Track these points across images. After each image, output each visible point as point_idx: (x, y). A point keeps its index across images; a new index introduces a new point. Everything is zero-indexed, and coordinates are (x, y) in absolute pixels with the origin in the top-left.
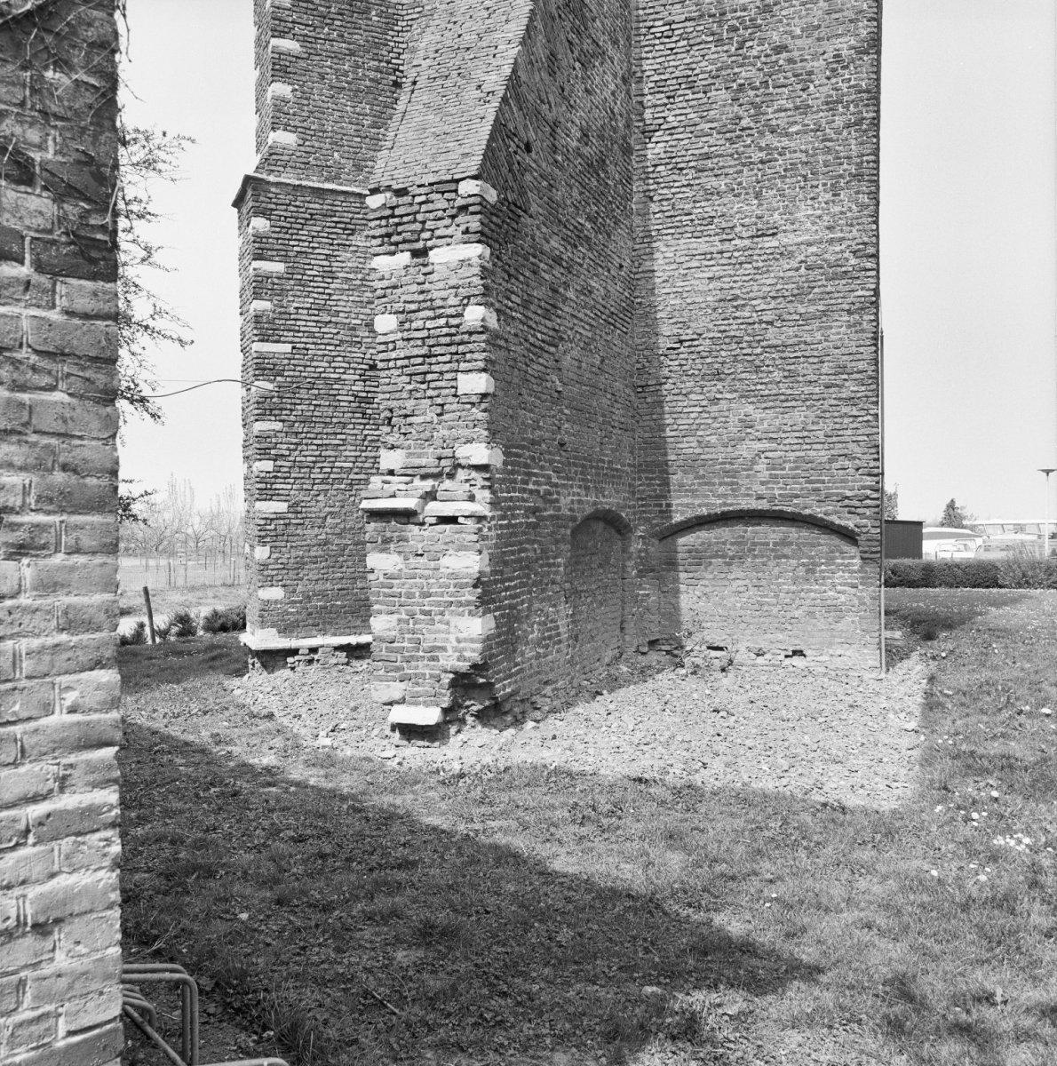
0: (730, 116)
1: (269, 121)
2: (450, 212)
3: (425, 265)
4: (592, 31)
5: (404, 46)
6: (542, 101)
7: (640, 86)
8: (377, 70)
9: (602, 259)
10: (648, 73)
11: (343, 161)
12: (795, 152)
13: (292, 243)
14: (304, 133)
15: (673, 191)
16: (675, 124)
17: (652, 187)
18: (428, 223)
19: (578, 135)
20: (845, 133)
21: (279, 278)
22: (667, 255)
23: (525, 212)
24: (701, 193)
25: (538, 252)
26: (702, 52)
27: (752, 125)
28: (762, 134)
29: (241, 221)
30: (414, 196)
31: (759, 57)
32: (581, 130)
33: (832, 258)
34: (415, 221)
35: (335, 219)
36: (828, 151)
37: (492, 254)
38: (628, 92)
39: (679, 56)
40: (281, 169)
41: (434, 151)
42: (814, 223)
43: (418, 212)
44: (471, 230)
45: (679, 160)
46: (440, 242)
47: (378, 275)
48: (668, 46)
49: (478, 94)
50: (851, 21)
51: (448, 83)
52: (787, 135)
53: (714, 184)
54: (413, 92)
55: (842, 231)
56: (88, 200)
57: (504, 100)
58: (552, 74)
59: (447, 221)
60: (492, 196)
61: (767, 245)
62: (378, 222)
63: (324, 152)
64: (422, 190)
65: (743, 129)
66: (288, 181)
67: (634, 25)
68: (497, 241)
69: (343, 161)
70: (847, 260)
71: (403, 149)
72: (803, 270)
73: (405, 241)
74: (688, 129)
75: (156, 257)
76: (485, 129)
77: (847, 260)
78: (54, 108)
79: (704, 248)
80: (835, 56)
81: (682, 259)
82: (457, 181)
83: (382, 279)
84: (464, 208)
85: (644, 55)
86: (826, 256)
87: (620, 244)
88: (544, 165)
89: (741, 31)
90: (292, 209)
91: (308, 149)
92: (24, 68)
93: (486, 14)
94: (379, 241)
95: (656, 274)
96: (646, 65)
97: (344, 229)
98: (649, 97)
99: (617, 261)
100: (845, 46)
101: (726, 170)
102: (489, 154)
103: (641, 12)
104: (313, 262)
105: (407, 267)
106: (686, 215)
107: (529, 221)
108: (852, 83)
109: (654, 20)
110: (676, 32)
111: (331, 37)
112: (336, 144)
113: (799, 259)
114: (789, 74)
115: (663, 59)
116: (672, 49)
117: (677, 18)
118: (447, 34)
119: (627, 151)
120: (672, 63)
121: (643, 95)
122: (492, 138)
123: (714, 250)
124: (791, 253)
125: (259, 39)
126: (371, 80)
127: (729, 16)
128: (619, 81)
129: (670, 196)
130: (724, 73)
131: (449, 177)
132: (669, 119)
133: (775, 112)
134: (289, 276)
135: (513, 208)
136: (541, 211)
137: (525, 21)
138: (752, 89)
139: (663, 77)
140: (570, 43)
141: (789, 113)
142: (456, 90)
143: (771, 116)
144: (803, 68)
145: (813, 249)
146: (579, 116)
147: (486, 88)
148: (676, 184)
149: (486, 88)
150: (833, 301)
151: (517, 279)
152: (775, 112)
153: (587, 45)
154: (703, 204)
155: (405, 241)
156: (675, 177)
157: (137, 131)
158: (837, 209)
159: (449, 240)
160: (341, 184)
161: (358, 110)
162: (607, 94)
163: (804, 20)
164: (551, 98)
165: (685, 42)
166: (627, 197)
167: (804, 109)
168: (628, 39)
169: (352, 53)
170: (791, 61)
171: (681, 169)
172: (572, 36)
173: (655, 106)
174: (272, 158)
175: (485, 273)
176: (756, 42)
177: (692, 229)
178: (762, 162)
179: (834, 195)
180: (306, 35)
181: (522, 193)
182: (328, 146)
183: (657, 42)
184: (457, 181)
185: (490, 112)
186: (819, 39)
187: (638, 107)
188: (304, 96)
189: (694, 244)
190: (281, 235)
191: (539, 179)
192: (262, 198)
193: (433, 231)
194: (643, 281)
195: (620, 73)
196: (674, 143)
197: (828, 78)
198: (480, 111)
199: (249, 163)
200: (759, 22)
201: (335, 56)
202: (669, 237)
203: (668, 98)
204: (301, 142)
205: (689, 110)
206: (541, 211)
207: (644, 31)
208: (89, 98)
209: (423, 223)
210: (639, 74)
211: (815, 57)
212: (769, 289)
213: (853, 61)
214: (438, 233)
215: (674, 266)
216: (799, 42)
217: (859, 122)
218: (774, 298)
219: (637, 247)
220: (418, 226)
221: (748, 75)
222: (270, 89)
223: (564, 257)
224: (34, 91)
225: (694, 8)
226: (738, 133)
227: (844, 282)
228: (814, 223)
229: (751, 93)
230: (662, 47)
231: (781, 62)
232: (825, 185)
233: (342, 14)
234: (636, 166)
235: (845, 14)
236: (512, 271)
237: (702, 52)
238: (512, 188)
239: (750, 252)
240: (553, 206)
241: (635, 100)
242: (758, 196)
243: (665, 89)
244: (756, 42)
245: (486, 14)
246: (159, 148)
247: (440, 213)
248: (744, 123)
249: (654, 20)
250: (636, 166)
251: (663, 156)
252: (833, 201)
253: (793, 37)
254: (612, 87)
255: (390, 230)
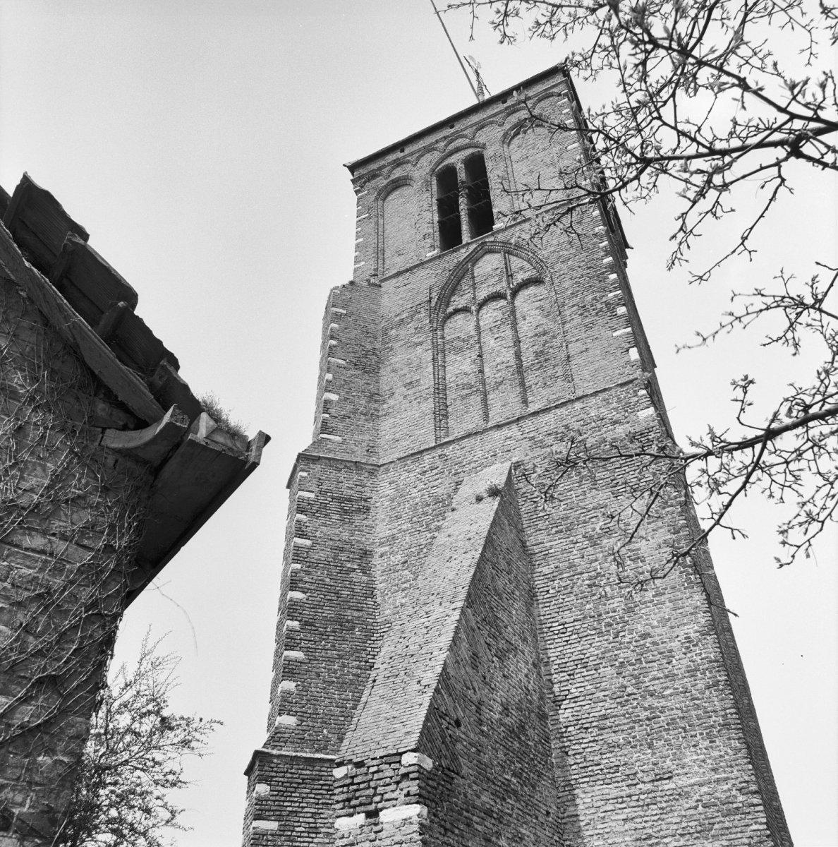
0: (618, 685)
1: (277, 708)
2: (394, 779)
3: (376, 824)
4: (505, 635)
5: (378, 650)
6: (468, 688)
7: (548, 668)
8: (358, 668)
9: (530, 807)
10: (551, 659)
11: (330, 736)
12: (672, 709)
13: (286, 804)
14: (302, 717)
15: (583, 747)
16: (577, 694)
17: (566, 744)
18: (379, 788)
19: (500, 709)
20: (707, 692)
21: (272, 835)
22: (586, 800)
23: (458, 774)
24: (606, 746)
25: (470, 807)
26: (589, 642)
27: (635, 691)
28: (644, 698)
29: (249, 787)
30: (368, 767)
31: (631, 643)
32: (502, 705)
33: (723, 796)
34: (369, 787)
35: (321, 782)
36: (698, 707)
37: (429, 812)
38: (539, 674)
39: (573, 646)
40: (283, 744)
41: (385, 731)
42: (700, 767)
43: (372, 780)
44: (411, 793)
45: (584, 721)
46: (388, 804)
47: (339, 834)
48: (564, 639)
49: (418, 687)
50: (692, 614)
51: (398, 680)
52: (663, 697)
53: (614, 739)
54: (373, 687)
55: (725, 772)
56: (40, 837)
57: (437, 690)
58: (475, 667)
59: (393, 787)
60: (428, 764)
61: (666, 787)
62: (341, 789)
63: (316, 729)
64: (375, 762)
65: (629, 695)
66: (287, 753)
67: (538, 627)
68: (433, 801)
69: (330, 736)
70: (735, 797)
71: (363, 731)
72: (700, 808)
73: (361, 804)
74: (588, 697)
75: (179, 819)
76: (422, 714)
77: (735, 797)
78: (37, 779)
79: (615, 793)
80: (686, 638)
81: (599, 804)
82: (401, 754)
83: (342, 837)
84: (405, 776)
85: (548, 647)
86: (716, 794)
87: (545, 792)
88: (472, 735)
89: (615, 626)
90: (289, 775)
91: (305, 728)
92: (26, 757)
93: (425, 631)
94: (341, 805)
95: (581, 818)
96: (550, 653)
97: (328, 790)
98: (555, 676)
99: (543, 809)
100: (692, 631)
101: (622, 727)
102: (426, 731)
103: (542, 618)
104: (301, 820)
105: (362, 826)
106: (596, 765)
107: (461, 781)
108: (703, 656)
109: (552, 622)
110: (569, 630)
111: (327, 647)
112: (325, 723)
113: (696, 798)
114: (656, 653)
115: (562, 648)
116: (567, 641)
117: (568, 620)
118: (399, 646)
119: (543, 717)
120: (568, 651)
121: (551, 674)
122: (427, 719)
123: (623, 794)
124: (687, 793)
125: (277, 651)
126: (353, 675)
127: (604, 616)
128: (530, 666)
129: (581, 751)
130: (607, 655)
131: (395, 751)
132: (572, 691)
133: (651, 680)
134: (282, 830)
135: (448, 772)
136: (471, 772)
137: (452, 634)
138: (630, 665)
139: (563, 661)
140: (489, 645)
141: (662, 681)
142: (403, 685)
143: (648, 684)
144: (665, 648)
145: (704, 789)
146: (500, 696)
147: (424, 682)
148: (585, 741)
149: (424, 682)
150: (733, 836)
151: (453, 832)
152: (651, 680)
153: (502, 644)
154: (608, 755)
155: (361, 804)
156: (584, 735)
157: (182, 718)
158: (716, 754)
159: (394, 802)
160: (327, 754)
161: (343, 697)
162: (521, 676)
163: (658, 615)
164: (475, 684)
165: (576, 636)
166: (547, 754)
167: (672, 677)
168: (535, 636)
169: (340, 657)
170: (654, 643)
171: (587, 728)
172: (489, 640)
173: (561, 682)
174: (277, 736)
175: (423, 829)
176: (627, 632)
177: (602, 777)
178: (648, 719)
179: (711, 742)
180: (309, 647)
181: (454, 758)
182: (319, 725)
183: (556, 637)
184: (401, 754)
185: (426, 700)
186: (672, 628)
187: (548, 683)
188: (304, 689)
189: (606, 790)
190: (278, 798)
191: (469, 746)
192: (266, 768)
193: (382, 795)
194: (569, 826)
195: (531, 661)
196: (578, 709)
197: (685, 654)
198: (419, 699)
199: (259, 740)
200: (626, 619)
201: (330, 660)
202: (585, 785)
203: (569, 675)
204: (299, 723)
205: (586, 683)
206: (471, 772)
207: (545, 630)
208: (61, 770)
209: (375, 788)
210: (546, 660)
211: (671, 639)
212: (675, 827)
213: (700, 641)
214: (386, 796)
215: (593, 810)
216: (658, 630)
217: (716, 684)
218: (682, 835)
219: (560, 795)
220: (371, 792)
221: (626, 655)
222: (280, 685)
223: (494, 809)
224: (28, 770)
225: (579, 613)
226: (626, 698)
227: (738, 817)
228: (700, 767)
229: (631, 668)
230: (560, 640)
231: (648, 645)
232: (701, 734)
233: (335, 632)
234: (551, 728)
235: (687, 609)
236: (448, 826)
237: (589, 642)
238: (445, 756)
239: (653, 794)
240: (482, 768)
241: (545, 678)
242: (650, 746)
243: (566, 669)
244: (627, 632)
245: (425, 631)
246: (196, 730)
247: (388, 780)
248: (629, 690)
249: (552, 622)
250: (551, 728)
251: (571, 719)
252: (712, 747)
253: (653, 627)
254: (526, 671)
255: (350, 796)
